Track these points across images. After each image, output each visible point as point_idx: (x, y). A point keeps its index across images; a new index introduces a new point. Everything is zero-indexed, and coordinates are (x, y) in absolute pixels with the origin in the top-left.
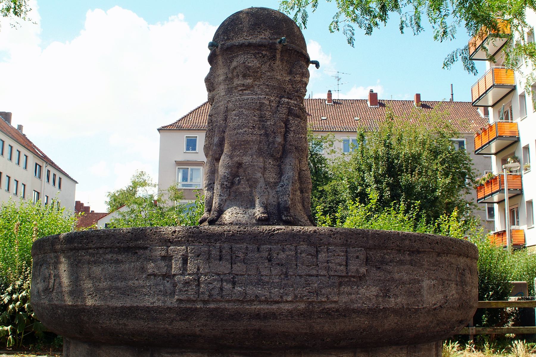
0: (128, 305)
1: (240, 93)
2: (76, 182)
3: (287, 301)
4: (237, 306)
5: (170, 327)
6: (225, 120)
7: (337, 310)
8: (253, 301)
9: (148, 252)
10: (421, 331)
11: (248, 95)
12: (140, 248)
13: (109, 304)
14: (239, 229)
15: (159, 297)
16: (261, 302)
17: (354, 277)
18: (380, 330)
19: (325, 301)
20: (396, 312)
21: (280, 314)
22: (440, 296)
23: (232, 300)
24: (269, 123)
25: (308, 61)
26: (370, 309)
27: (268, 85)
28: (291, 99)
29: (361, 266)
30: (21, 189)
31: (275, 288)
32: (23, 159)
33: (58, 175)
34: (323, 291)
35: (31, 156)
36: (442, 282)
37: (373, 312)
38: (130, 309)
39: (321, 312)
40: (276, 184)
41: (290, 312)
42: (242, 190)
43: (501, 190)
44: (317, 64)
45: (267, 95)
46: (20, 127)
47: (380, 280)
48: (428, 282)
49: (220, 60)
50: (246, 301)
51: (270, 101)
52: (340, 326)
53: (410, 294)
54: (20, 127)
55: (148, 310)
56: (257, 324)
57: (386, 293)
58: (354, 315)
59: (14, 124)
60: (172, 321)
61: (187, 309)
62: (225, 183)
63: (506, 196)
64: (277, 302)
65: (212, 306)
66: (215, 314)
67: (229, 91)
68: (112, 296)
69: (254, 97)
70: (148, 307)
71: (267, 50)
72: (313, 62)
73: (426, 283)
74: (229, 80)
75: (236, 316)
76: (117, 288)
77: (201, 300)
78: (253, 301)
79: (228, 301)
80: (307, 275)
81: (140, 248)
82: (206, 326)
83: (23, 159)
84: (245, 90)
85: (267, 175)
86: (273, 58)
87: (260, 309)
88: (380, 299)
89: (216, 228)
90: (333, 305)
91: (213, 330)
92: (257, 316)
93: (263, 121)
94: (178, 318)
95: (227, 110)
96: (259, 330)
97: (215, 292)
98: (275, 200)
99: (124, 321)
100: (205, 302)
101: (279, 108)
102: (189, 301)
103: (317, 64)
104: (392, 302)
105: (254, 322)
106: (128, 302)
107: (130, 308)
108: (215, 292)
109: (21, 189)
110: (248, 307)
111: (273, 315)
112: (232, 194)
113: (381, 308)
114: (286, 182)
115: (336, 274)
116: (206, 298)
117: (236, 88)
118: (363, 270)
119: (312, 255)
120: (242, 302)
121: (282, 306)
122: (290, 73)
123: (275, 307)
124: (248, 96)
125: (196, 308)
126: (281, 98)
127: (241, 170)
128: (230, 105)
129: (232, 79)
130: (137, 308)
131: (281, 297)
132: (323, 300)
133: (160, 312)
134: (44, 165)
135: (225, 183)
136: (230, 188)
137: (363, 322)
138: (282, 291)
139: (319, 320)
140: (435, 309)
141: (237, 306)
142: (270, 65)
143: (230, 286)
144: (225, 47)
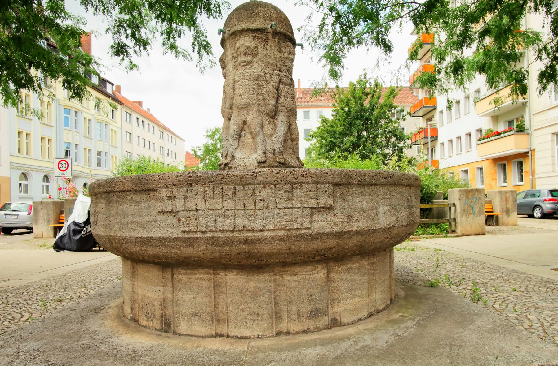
0: (146, 236)
1: (243, 67)
2: (184, 141)
3: (269, 230)
4: (229, 235)
5: (179, 252)
6: (234, 89)
7: (311, 235)
8: (242, 230)
9: (157, 193)
10: (379, 245)
11: (249, 69)
12: (151, 190)
13: (132, 235)
14: (228, 173)
15: (168, 229)
16: (248, 231)
17: (323, 208)
18: (346, 247)
19: (300, 228)
20: (358, 233)
21: (264, 240)
22: (393, 218)
23: (224, 231)
24: (265, 90)
25: (294, 43)
26: (337, 233)
27: (263, 61)
28: (282, 72)
29: (329, 198)
30: (152, 145)
31: (258, 220)
32: (151, 128)
33: (174, 137)
34: (298, 220)
35: (156, 127)
36: (394, 206)
37: (340, 235)
38: (147, 239)
39: (298, 236)
40: (272, 135)
41: (273, 238)
42: (247, 141)
43: (426, 138)
44: (302, 46)
45: (263, 68)
46: (149, 110)
47: (345, 209)
48: (384, 208)
49: (228, 44)
50: (236, 231)
51: (265, 73)
52: (316, 245)
53: (369, 217)
54: (149, 110)
55: (160, 240)
56: (246, 248)
57: (350, 218)
58: (325, 238)
59: (145, 107)
60: (180, 247)
61: (190, 238)
62: (235, 136)
63: (429, 140)
64: (261, 231)
65: (209, 235)
66: (214, 241)
67: (235, 67)
68: (134, 229)
69: (253, 70)
70: (160, 238)
71: (262, 34)
72: (299, 45)
73: (382, 209)
74: (235, 58)
75: (228, 242)
76: (138, 223)
77: (200, 231)
78: (242, 230)
79: (222, 231)
80: (285, 208)
81: (151, 190)
82: (206, 250)
83: (151, 128)
84: (246, 65)
85: (265, 129)
86: (267, 40)
87: (248, 237)
88: (345, 224)
89: (225, 172)
90: (307, 231)
91: (213, 253)
92: (246, 242)
93: (261, 89)
94: (184, 245)
95: (235, 82)
96: (249, 252)
97: (211, 224)
98: (271, 147)
99: (144, 248)
100: (203, 232)
101: (272, 79)
102: (190, 232)
103: (302, 46)
104: (355, 226)
105: (244, 247)
106: (144, 234)
107: (147, 238)
108: (211, 224)
109: (152, 145)
110: (238, 235)
111: (259, 241)
112: (241, 144)
113: (346, 231)
114: (279, 134)
115: (309, 206)
116: (204, 229)
117: (240, 64)
118: (330, 202)
119: (288, 192)
120: (233, 231)
121: (266, 233)
122: (280, 51)
123: (260, 234)
124: (248, 70)
125: (197, 238)
126: (273, 71)
127: (246, 126)
128: (237, 78)
129: (237, 57)
130: (152, 238)
131: (264, 226)
132: (299, 227)
133: (170, 241)
134: (164, 132)
135: (235, 136)
136: (238, 139)
137: (333, 242)
138: (264, 222)
139: (296, 243)
140: (389, 228)
141: (229, 235)
142: (264, 45)
143: (222, 218)
144: (230, 32)
